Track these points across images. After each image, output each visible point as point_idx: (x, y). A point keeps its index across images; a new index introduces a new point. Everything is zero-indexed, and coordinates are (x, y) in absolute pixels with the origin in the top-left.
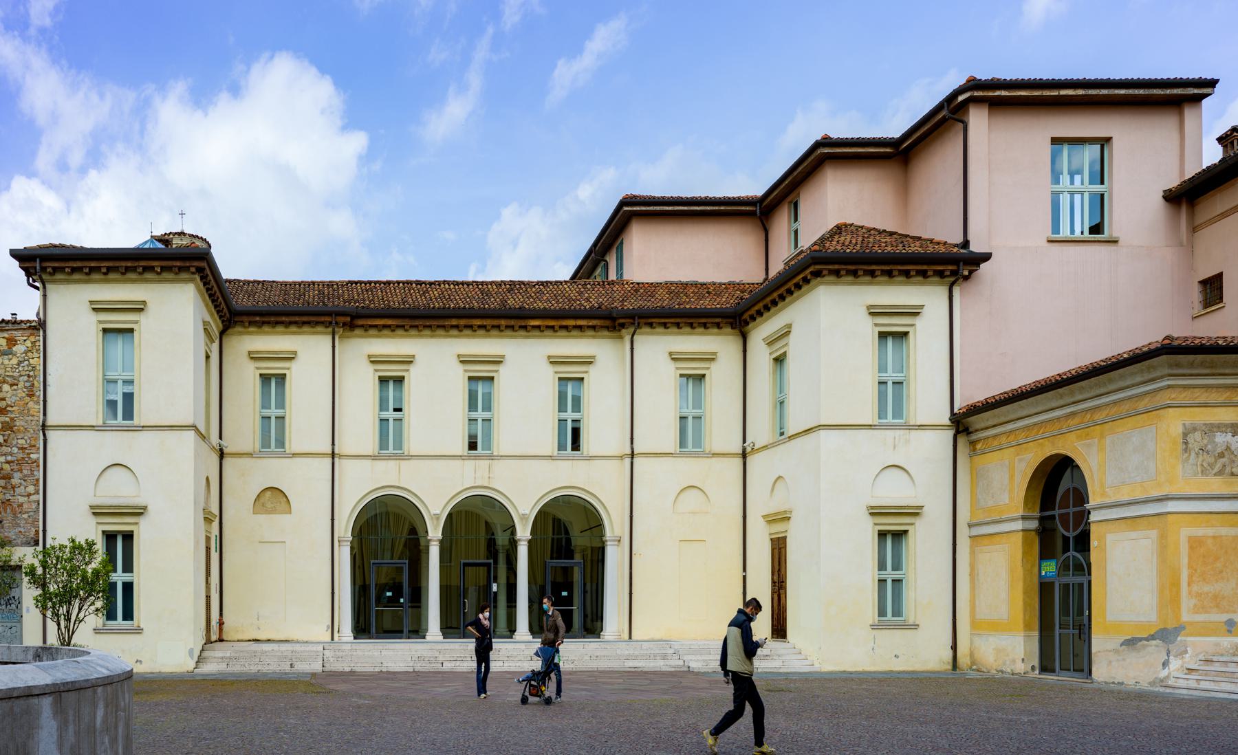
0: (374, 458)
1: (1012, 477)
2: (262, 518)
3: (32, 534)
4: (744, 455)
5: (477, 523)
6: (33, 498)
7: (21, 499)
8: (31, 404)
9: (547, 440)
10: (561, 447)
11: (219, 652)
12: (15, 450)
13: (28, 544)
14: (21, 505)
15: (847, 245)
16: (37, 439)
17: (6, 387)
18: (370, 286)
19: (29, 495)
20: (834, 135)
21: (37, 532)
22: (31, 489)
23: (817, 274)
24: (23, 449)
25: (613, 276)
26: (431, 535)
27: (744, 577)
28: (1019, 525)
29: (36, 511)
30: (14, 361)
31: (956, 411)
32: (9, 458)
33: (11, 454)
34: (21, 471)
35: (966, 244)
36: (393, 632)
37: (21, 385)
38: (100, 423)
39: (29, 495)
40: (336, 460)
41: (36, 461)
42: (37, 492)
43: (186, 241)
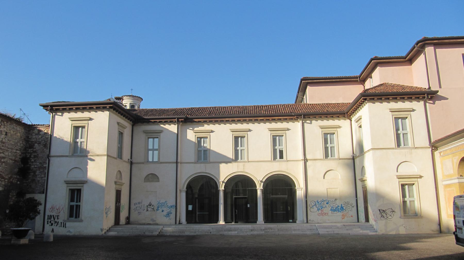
0: (195, 163)
1: (453, 164)
2: (148, 183)
3: (42, 190)
4: (177, 163)
5: (241, 184)
6: (43, 179)
7: (39, 179)
8: (45, 150)
9: (268, 154)
10: (275, 158)
11: (118, 228)
12: (38, 164)
13: (40, 193)
14: (39, 181)
15: (382, 90)
16: (46, 160)
17: (36, 145)
18: (328, 105)
19: (42, 178)
20: (379, 56)
21: (44, 189)
22: (43, 176)
23: (366, 99)
24: (41, 163)
25: (305, 102)
26: (258, 187)
27: (357, 200)
28: (457, 181)
29: (44, 183)
30: (40, 137)
31: (432, 141)
32: (36, 166)
33: (37, 165)
34: (39, 170)
35: (429, 88)
36: (203, 221)
37: (42, 144)
38: (71, 154)
39: (42, 178)
40: (179, 165)
41: (45, 167)
42: (45, 177)
43: (419, 90)
